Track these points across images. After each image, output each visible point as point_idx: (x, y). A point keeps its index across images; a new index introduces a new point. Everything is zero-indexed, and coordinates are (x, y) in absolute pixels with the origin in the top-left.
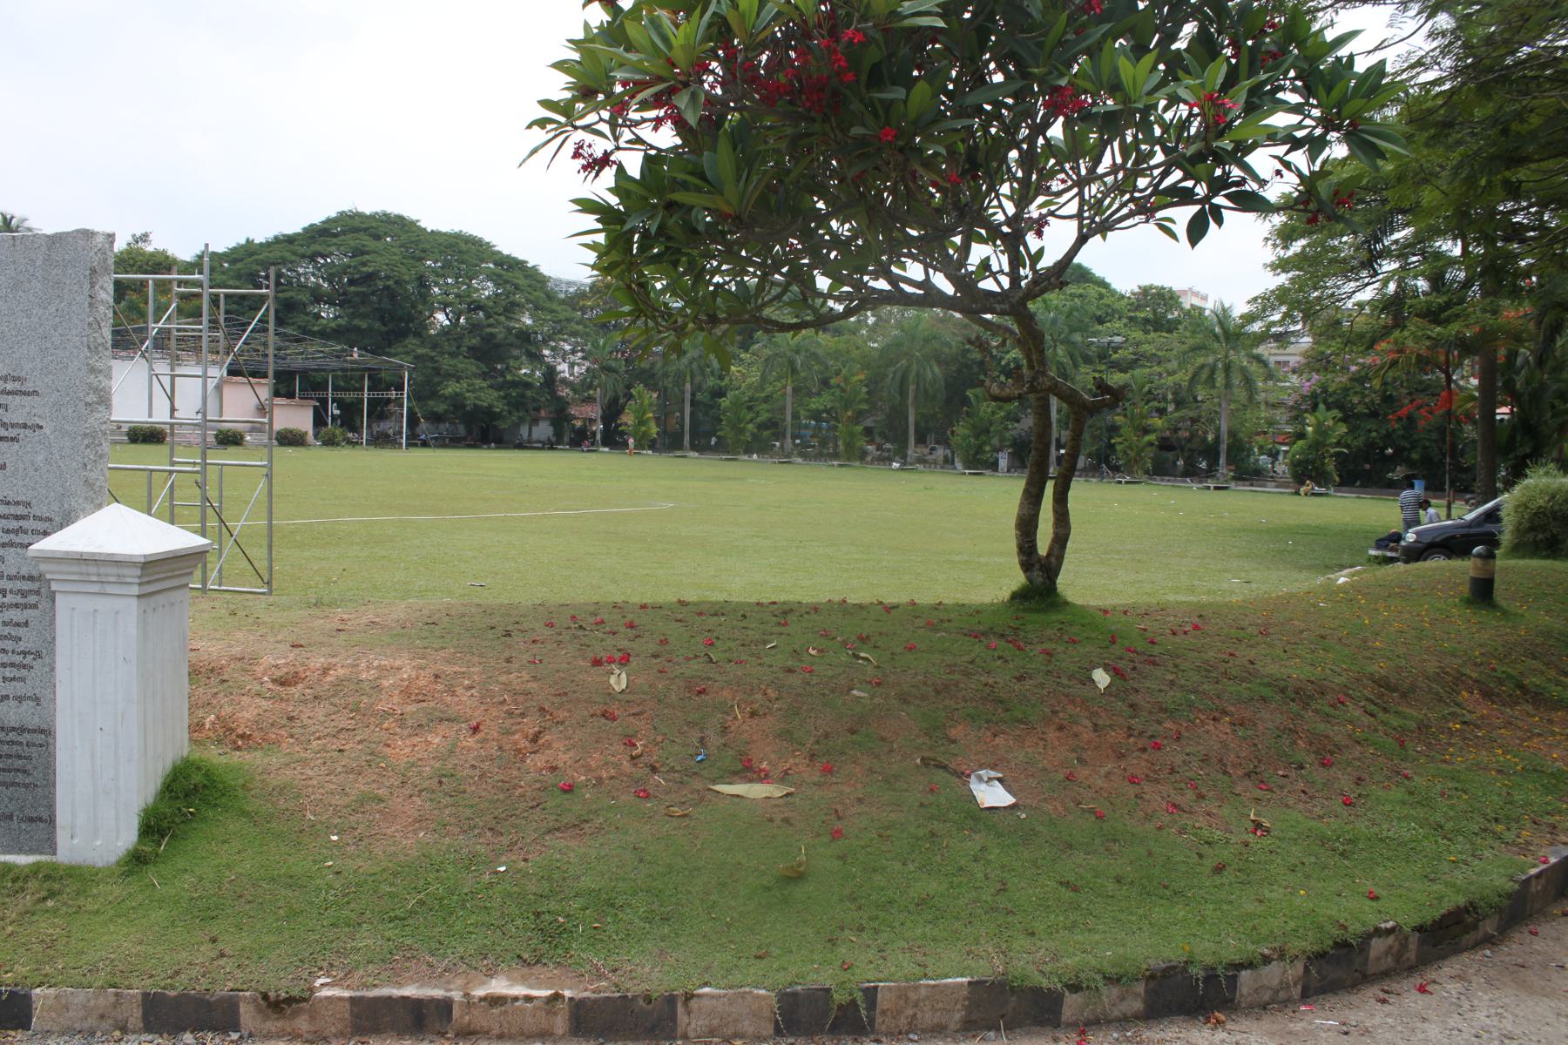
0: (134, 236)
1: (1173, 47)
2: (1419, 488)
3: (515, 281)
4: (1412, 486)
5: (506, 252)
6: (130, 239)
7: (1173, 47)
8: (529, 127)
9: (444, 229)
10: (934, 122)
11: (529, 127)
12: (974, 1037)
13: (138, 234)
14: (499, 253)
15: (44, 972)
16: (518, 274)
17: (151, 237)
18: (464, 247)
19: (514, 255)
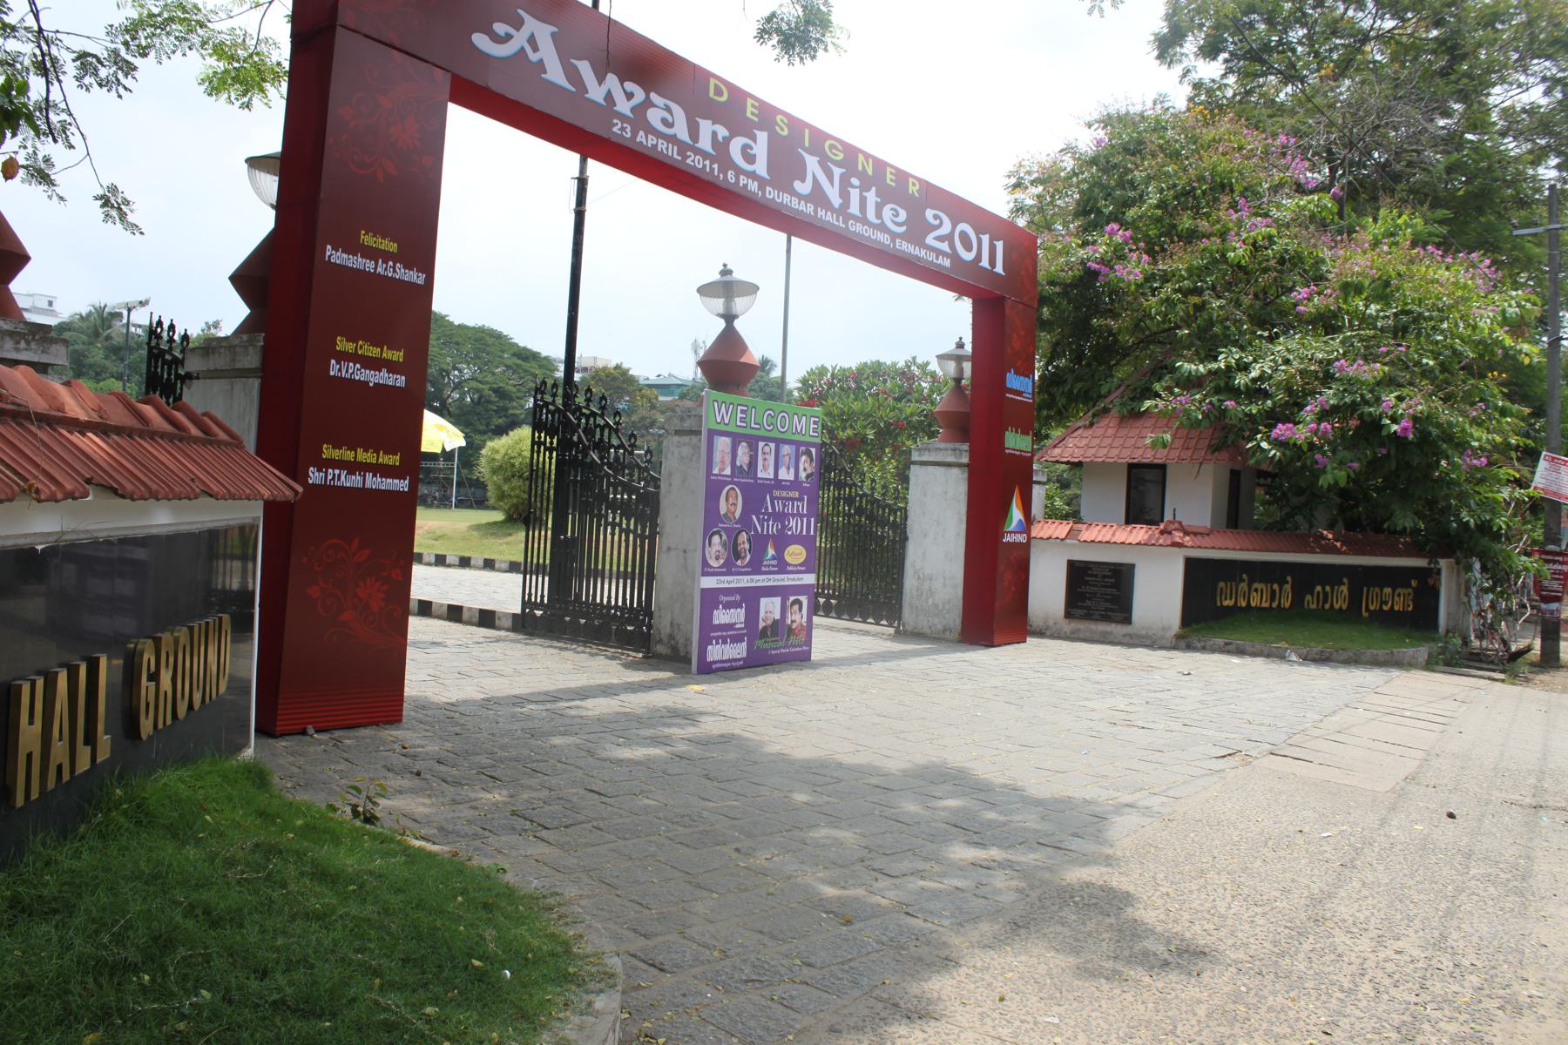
0: (207, 323)
1: (874, 189)
2: (424, 464)
3: (533, 370)
4: (1266, 479)
5: (521, 344)
6: (204, 326)
7: (874, 189)
8: (134, 228)
9: (471, 324)
10: (1550, 213)
11: (134, 228)
12: (725, 740)
13: (211, 323)
14: (516, 345)
15: (401, 897)
16: (534, 364)
17: (222, 324)
18: (490, 341)
19: (529, 347)
